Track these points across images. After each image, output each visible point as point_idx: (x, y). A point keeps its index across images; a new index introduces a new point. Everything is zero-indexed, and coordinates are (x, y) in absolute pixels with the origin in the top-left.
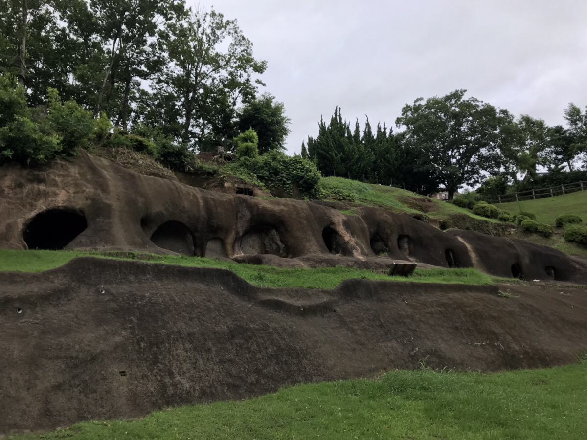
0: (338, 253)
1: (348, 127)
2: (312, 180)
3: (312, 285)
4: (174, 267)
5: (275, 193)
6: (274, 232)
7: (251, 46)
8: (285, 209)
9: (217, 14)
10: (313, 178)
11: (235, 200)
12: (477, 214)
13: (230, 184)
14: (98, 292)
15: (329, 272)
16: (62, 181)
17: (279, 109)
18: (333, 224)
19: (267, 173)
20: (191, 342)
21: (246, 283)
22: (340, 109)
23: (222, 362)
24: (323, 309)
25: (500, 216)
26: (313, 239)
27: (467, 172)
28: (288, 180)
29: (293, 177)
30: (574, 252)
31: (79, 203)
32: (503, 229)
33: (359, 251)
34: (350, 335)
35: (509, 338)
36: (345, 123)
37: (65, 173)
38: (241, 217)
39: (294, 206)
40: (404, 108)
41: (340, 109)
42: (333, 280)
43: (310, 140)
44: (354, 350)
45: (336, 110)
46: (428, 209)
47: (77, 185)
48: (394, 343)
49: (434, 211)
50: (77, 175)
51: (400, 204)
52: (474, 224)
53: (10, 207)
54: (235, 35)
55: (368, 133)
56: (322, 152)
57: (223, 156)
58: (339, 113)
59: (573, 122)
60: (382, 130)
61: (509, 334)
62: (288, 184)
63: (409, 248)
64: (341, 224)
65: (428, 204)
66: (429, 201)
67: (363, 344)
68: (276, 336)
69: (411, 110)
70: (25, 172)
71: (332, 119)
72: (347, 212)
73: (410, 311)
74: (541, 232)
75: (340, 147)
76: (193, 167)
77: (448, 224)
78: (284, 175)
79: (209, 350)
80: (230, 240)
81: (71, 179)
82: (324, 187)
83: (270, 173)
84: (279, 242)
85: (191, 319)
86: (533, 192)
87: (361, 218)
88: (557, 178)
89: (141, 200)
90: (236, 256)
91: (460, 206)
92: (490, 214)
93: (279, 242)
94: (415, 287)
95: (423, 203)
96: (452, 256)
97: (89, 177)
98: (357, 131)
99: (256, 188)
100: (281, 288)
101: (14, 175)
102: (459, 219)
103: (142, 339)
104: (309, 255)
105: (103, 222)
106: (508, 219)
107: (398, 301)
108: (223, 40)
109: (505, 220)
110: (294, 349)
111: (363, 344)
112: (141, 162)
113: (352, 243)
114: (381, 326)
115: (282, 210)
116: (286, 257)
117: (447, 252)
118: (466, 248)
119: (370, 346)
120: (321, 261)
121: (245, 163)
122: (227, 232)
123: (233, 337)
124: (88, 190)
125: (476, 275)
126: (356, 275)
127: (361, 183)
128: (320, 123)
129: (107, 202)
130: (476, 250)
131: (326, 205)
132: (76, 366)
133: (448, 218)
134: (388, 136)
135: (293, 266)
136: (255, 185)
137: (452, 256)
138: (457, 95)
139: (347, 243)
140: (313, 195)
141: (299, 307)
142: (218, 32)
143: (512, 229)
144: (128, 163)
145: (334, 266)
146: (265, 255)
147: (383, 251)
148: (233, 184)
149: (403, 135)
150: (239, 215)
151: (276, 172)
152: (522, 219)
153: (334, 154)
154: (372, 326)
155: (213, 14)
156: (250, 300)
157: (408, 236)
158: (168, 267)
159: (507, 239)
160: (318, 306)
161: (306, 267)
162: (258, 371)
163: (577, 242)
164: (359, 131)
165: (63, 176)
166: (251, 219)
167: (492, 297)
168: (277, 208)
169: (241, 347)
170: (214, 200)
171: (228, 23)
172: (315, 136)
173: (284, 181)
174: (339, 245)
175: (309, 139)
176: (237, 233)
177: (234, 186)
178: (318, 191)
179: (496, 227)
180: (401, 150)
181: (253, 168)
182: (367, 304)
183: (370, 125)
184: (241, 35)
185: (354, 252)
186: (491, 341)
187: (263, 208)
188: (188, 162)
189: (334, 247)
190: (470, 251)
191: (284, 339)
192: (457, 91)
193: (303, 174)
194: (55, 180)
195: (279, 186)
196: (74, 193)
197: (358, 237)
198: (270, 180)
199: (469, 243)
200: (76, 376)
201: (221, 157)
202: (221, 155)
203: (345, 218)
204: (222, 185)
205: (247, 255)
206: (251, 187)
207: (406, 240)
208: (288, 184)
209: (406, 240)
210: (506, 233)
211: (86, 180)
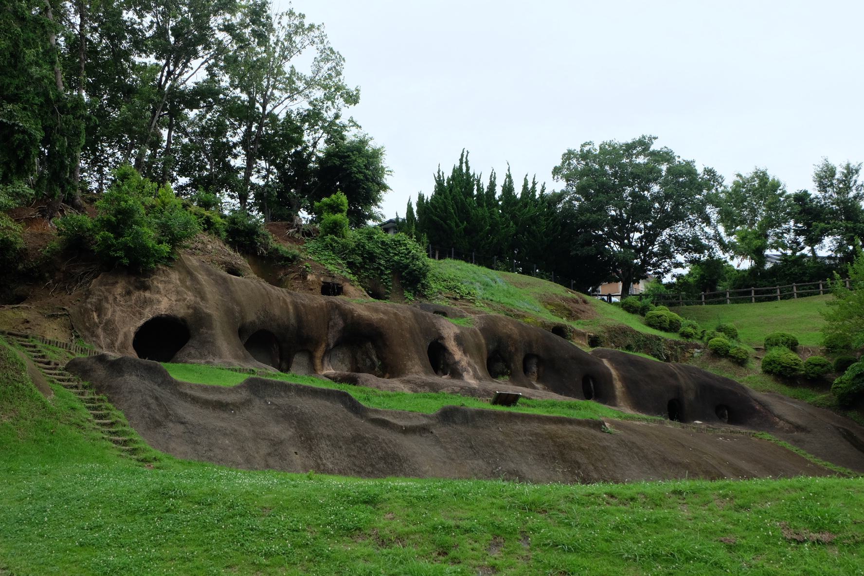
0: (445, 374)
1: (479, 181)
2: (419, 272)
3: (412, 409)
4: (308, 387)
5: (368, 285)
6: (369, 345)
7: (342, 62)
8: (385, 318)
9: (297, 14)
10: (421, 269)
11: (326, 307)
12: (650, 325)
13: (314, 276)
14: (266, 402)
15: (431, 398)
16: (164, 288)
17: (376, 154)
18: (442, 338)
19: (360, 259)
20: (330, 441)
21: (359, 403)
22: (468, 153)
23: (349, 456)
24: (422, 430)
25: (681, 330)
26: (417, 361)
27: (656, 255)
28: (386, 268)
29: (393, 265)
30: (767, 387)
31: (181, 311)
32: (681, 348)
33: (471, 373)
34: (443, 451)
35: (591, 467)
36: (474, 174)
37: (166, 279)
38: (332, 326)
39: (395, 314)
40: (564, 155)
41: (468, 153)
42: (433, 405)
43: (421, 197)
44: (444, 463)
45: (462, 155)
46: (580, 315)
47: (178, 293)
48: (480, 462)
49: (587, 318)
50: (178, 282)
51: (539, 307)
52: (639, 341)
53: (123, 315)
54: (321, 46)
55: (508, 189)
56: (436, 218)
57: (301, 230)
58: (466, 158)
59: (823, 187)
60: (530, 186)
61: (593, 465)
62: (385, 274)
63: (538, 371)
64: (452, 339)
65: (582, 306)
66: (585, 302)
67: (453, 460)
68: (384, 445)
69: (575, 156)
70: (133, 279)
71: (454, 169)
72: (461, 322)
73: (501, 437)
74: (733, 357)
75: (463, 211)
76: (266, 249)
77: (601, 339)
78: (382, 262)
79: (341, 447)
80: (319, 354)
81: (172, 286)
82: (437, 279)
83: (364, 258)
84: (375, 359)
85: (328, 426)
86: (753, 291)
87: (479, 331)
88: (791, 272)
89: (237, 308)
90: (325, 372)
91: (629, 311)
92: (668, 326)
93: (375, 359)
94: (511, 416)
95: (576, 305)
96: (592, 385)
97: (188, 283)
98: (492, 185)
99: (347, 284)
100: (387, 410)
101: (123, 282)
102: (617, 333)
103: (302, 435)
104: (410, 377)
105: (207, 333)
106: (692, 334)
107: (493, 429)
108: (303, 51)
109: (687, 336)
110: (398, 455)
111: (453, 460)
112: (210, 247)
113: (464, 363)
114: (471, 447)
115: (381, 319)
116: (383, 377)
117: (586, 379)
118: (610, 375)
119: (459, 462)
120: (423, 385)
121: (331, 245)
122: (317, 344)
123: (355, 442)
124: (188, 298)
125: (591, 409)
126: (456, 402)
127: (490, 270)
128: (437, 175)
129: (208, 311)
130: (624, 379)
131: (436, 312)
132: (274, 445)
133: (602, 331)
134: (537, 196)
135: (393, 389)
136: (345, 279)
137: (592, 385)
138: (643, 145)
139: (457, 363)
140: (419, 291)
141: (402, 427)
142: (297, 39)
143: (696, 350)
144: (195, 249)
145: (437, 392)
146: (361, 375)
147: (503, 374)
148: (318, 276)
149: (559, 197)
150: (331, 323)
151: (371, 257)
152: (712, 336)
153: (453, 225)
154: (463, 447)
155: (291, 13)
156: (362, 418)
157: (537, 356)
158: (305, 387)
159: (692, 364)
160: (417, 427)
161: (406, 390)
162: (372, 465)
163: (774, 374)
164: (496, 185)
165: (165, 282)
166: (344, 329)
167: (593, 431)
168: (375, 317)
169: (360, 448)
170: (303, 305)
171: (312, 27)
172: (429, 192)
173: (381, 270)
174: (447, 365)
175: (420, 195)
176: (328, 345)
177: (319, 279)
178: (427, 285)
179: (672, 345)
180: (553, 220)
181: (343, 252)
182: (462, 429)
183: (513, 178)
184: (329, 48)
185: (465, 374)
186: (572, 468)
187: (359, 315)
188: (261, 243)
189: (442, 366)
190: (615, 379)
191: (390, 447)
192: (644, 137)
193: (408, 261)
194: (157, 287)
195: (374, 276)
196: (176, 301)
197: (472, 356)
198: (362, 267)
199: (616, 369)
200: (276, 450)
201: (297, 232)
202: (299, 229)
203: (458, 331)
204: (305, 278)
205: (338, 372)
206: (341, 282)
207: (534, 361)
208: (385, 274)
209: (534, 361)
210: (687, 355)
211: (187, 288)
